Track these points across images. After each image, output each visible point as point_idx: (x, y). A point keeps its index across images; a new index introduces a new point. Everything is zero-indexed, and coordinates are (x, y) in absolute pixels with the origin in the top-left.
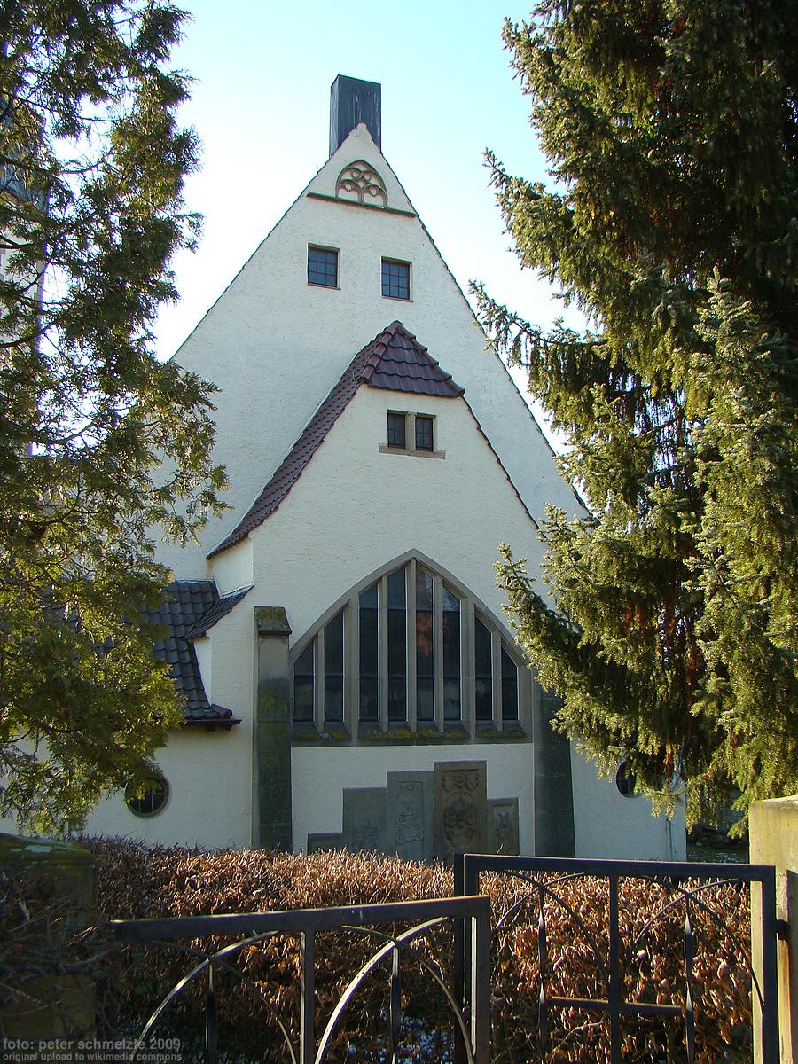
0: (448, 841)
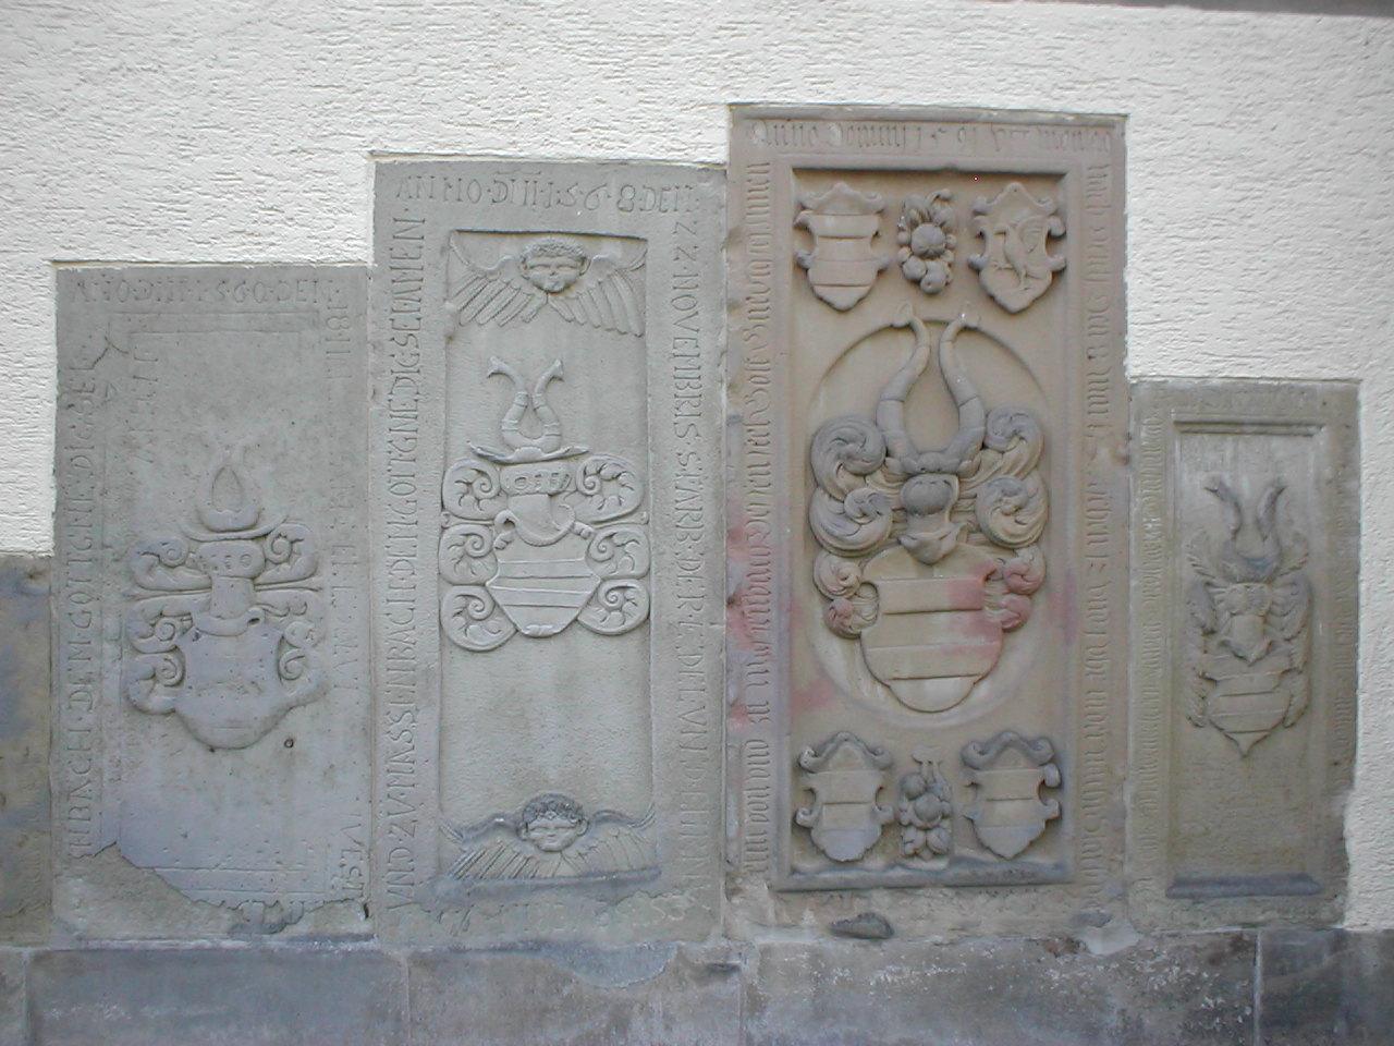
0: (835, 652)
